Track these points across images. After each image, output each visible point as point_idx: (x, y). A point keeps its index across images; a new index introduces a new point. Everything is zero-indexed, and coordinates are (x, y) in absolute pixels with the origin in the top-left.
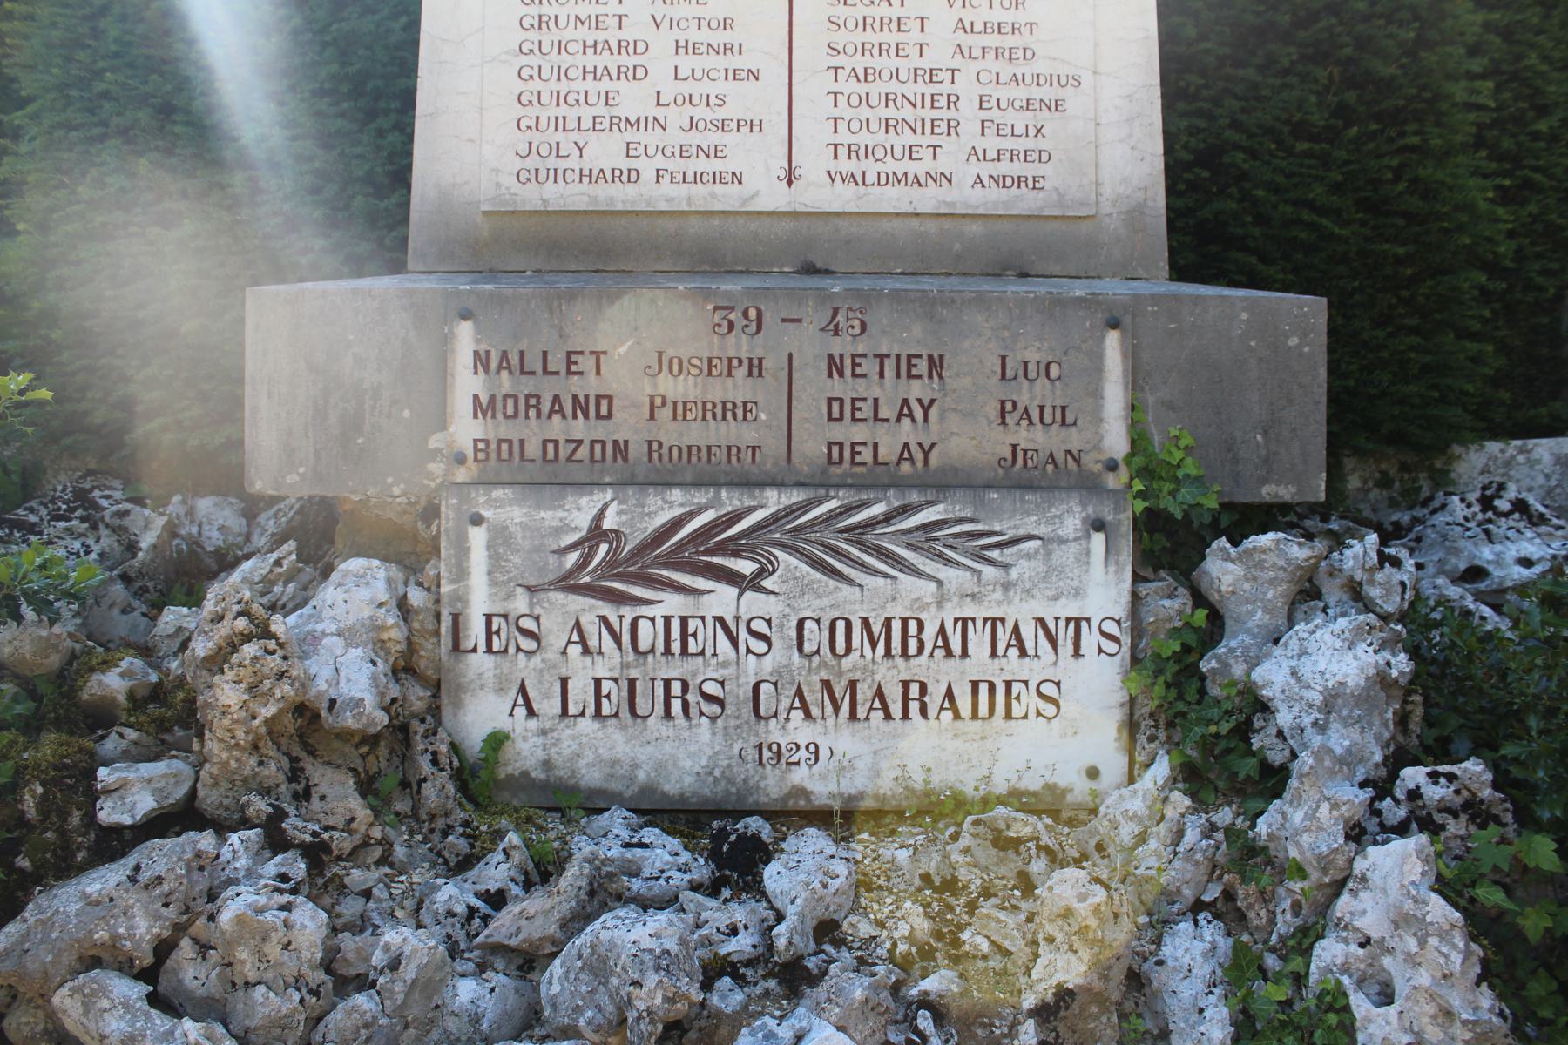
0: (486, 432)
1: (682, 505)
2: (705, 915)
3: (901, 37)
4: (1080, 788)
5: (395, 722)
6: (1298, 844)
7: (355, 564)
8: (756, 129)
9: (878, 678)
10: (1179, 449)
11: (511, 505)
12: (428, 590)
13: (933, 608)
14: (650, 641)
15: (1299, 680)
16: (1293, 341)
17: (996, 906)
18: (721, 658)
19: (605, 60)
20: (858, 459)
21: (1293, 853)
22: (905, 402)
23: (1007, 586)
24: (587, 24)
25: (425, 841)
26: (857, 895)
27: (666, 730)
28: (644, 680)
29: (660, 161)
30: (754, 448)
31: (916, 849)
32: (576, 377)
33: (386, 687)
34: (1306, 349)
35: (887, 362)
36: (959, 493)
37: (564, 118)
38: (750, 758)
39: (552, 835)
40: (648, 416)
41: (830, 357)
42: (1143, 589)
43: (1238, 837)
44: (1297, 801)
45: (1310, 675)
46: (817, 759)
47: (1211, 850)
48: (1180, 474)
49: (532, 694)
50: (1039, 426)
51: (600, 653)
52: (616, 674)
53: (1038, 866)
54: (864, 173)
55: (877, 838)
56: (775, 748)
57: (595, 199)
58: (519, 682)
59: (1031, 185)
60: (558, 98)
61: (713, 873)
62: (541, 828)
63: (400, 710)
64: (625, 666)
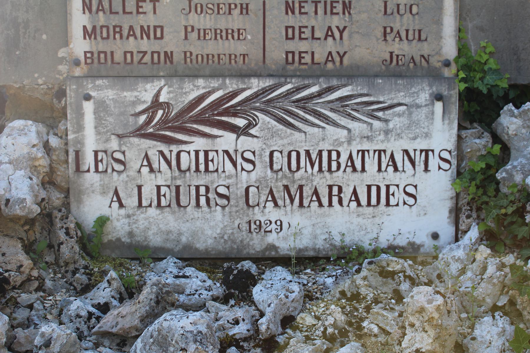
0: (91, 47)
1: (204, 88)
4: (428, 243)
5: (44, 212)
7: (18, 123)
9: (315, 183)
10: (486, 53)
11: (107, 89)
12: (61, 137)
13: (345, 145)
14: (188, 164)
18: (227, 174)
20: (303, 61)
22: (330, 28)
25: (63, 278)
27: (197, 214)
28: (185, 186)
30: (244, 55)
31: (337, 277)
32: (142, 15)
33: (38, 192)
36: (360, 80)
38: (244, 229)
39: (135, 273)
40: (184, 38)
42: (464, 133)
46: (281, 229)
47: (502, 277)
49: (121, 195)
50: (406, 41)
51: (160, 171)
52: (169, 183)
55: (315, 272)
56: (258, 223)
58: (114, 188)
61: (225, 291)
63: (47, 205)
64: (173, 178)
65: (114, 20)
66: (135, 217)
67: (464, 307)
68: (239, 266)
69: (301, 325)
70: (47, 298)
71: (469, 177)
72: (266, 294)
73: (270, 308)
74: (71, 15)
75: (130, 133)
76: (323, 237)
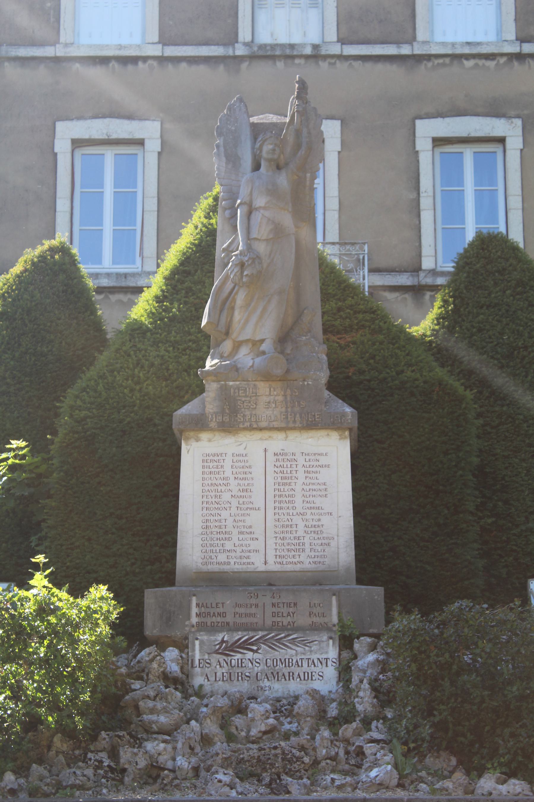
3: (292, 529)
7: (171, 648)
16: (376, 597)
19: (222, 536)
22: (289, 613)
23: (311, 651)
27: (238, 683)
29: (235, 560)
30: (256, 623)
41: (273, 603)
49: (209, 676)
64: (229, 670)
65: (208, 610)
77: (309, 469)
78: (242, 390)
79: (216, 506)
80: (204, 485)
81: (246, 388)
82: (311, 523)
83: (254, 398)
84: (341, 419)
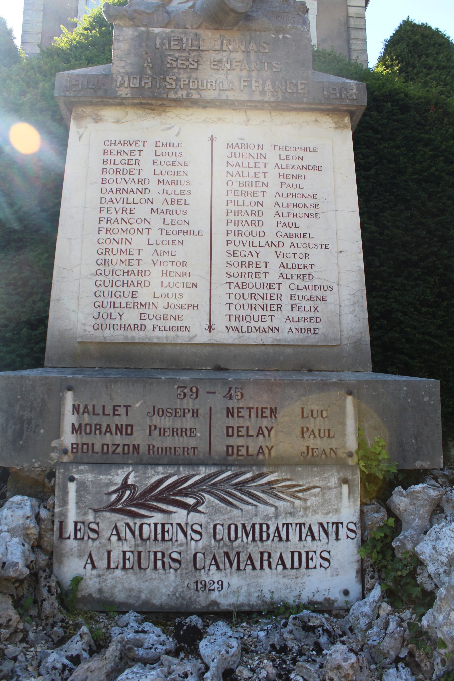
0: (77, 440)
1: (163, 473)
2: (173, 667)
3: (257, 270)
4: (340, 599)
5: (32, 571)
6: (442, 631)
7: (17, 498)
8: (196, 308)
9: (249, 550)
10: (379, 446)
11: (87, 473)
12: (49, 510)
13: (273, 519)
14: (148, 534)
15: (436, 551)
16: (426, 399)
17: (305, 661)
18: (179, 542)
20: (240, 453)
21: (440, 635)
22: (260, 428)
24: (125, 263)
25: (43, 630)
26: (242, 656)
27: (154, 575)
28: (145, 552)
29: (154, 322)
30: (194, 448)
31: (268, 631)
32: (117, 417)
33: (29, 556)
34: (432, 402)
35: (252, 411)
36: (284, 468)
37: (114, 302)
38: (192, 587)
39: (102, 625)
40: (148, 434)
41: (228, 408)
42: (365, 509)
43: (414, 626)
44: (440, 610)
45: (441, 549)
46: (222, 588)
47: (402, 632)
48: (380, 457)
49: (94, 558)
50: (318, 438)
51: (126, 540)
52: (132, 549)
53: (323, 640)
54: (242, 327)
55: (250, 625)
56: (203, 583)
57: (126, 337)
58: (89, 553)
59: (313, 332)
60: (112, 294)
61: (176, 645)
62: (97, 622)
63: (34, 566)
64: (136, 545)
65: (96, 420)
66: (104, 577)
67: (372, 658)
68: (188, 620)
69: (239, 678)
70: (29, 650)
71: (371, 544)
72: (210, 649)
73: (214, 663)
74: (63, 415)
75: (104, 508)
76: (256, 595)
77: (287, 172)
78: (175, 40)
79: (124, 226)
80: (104, 191)
81: (182, 39)
82: (290, 261)
83: (194, 54)
84: (340, 94)
